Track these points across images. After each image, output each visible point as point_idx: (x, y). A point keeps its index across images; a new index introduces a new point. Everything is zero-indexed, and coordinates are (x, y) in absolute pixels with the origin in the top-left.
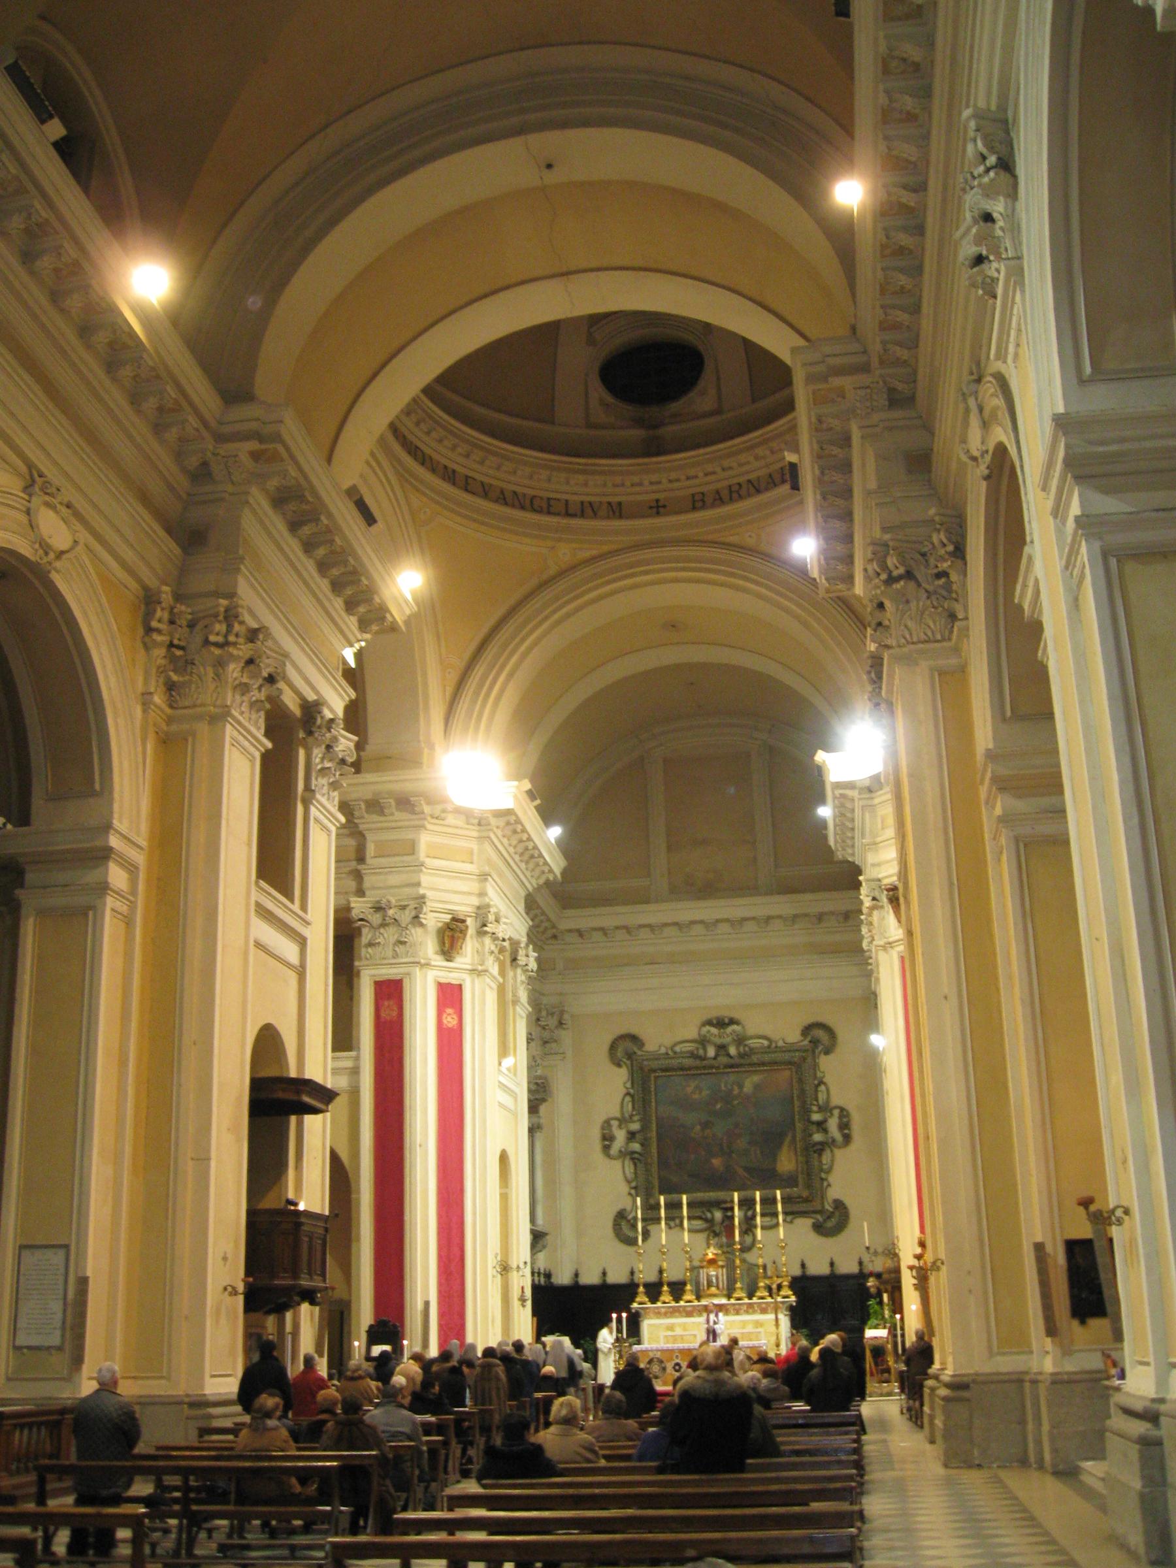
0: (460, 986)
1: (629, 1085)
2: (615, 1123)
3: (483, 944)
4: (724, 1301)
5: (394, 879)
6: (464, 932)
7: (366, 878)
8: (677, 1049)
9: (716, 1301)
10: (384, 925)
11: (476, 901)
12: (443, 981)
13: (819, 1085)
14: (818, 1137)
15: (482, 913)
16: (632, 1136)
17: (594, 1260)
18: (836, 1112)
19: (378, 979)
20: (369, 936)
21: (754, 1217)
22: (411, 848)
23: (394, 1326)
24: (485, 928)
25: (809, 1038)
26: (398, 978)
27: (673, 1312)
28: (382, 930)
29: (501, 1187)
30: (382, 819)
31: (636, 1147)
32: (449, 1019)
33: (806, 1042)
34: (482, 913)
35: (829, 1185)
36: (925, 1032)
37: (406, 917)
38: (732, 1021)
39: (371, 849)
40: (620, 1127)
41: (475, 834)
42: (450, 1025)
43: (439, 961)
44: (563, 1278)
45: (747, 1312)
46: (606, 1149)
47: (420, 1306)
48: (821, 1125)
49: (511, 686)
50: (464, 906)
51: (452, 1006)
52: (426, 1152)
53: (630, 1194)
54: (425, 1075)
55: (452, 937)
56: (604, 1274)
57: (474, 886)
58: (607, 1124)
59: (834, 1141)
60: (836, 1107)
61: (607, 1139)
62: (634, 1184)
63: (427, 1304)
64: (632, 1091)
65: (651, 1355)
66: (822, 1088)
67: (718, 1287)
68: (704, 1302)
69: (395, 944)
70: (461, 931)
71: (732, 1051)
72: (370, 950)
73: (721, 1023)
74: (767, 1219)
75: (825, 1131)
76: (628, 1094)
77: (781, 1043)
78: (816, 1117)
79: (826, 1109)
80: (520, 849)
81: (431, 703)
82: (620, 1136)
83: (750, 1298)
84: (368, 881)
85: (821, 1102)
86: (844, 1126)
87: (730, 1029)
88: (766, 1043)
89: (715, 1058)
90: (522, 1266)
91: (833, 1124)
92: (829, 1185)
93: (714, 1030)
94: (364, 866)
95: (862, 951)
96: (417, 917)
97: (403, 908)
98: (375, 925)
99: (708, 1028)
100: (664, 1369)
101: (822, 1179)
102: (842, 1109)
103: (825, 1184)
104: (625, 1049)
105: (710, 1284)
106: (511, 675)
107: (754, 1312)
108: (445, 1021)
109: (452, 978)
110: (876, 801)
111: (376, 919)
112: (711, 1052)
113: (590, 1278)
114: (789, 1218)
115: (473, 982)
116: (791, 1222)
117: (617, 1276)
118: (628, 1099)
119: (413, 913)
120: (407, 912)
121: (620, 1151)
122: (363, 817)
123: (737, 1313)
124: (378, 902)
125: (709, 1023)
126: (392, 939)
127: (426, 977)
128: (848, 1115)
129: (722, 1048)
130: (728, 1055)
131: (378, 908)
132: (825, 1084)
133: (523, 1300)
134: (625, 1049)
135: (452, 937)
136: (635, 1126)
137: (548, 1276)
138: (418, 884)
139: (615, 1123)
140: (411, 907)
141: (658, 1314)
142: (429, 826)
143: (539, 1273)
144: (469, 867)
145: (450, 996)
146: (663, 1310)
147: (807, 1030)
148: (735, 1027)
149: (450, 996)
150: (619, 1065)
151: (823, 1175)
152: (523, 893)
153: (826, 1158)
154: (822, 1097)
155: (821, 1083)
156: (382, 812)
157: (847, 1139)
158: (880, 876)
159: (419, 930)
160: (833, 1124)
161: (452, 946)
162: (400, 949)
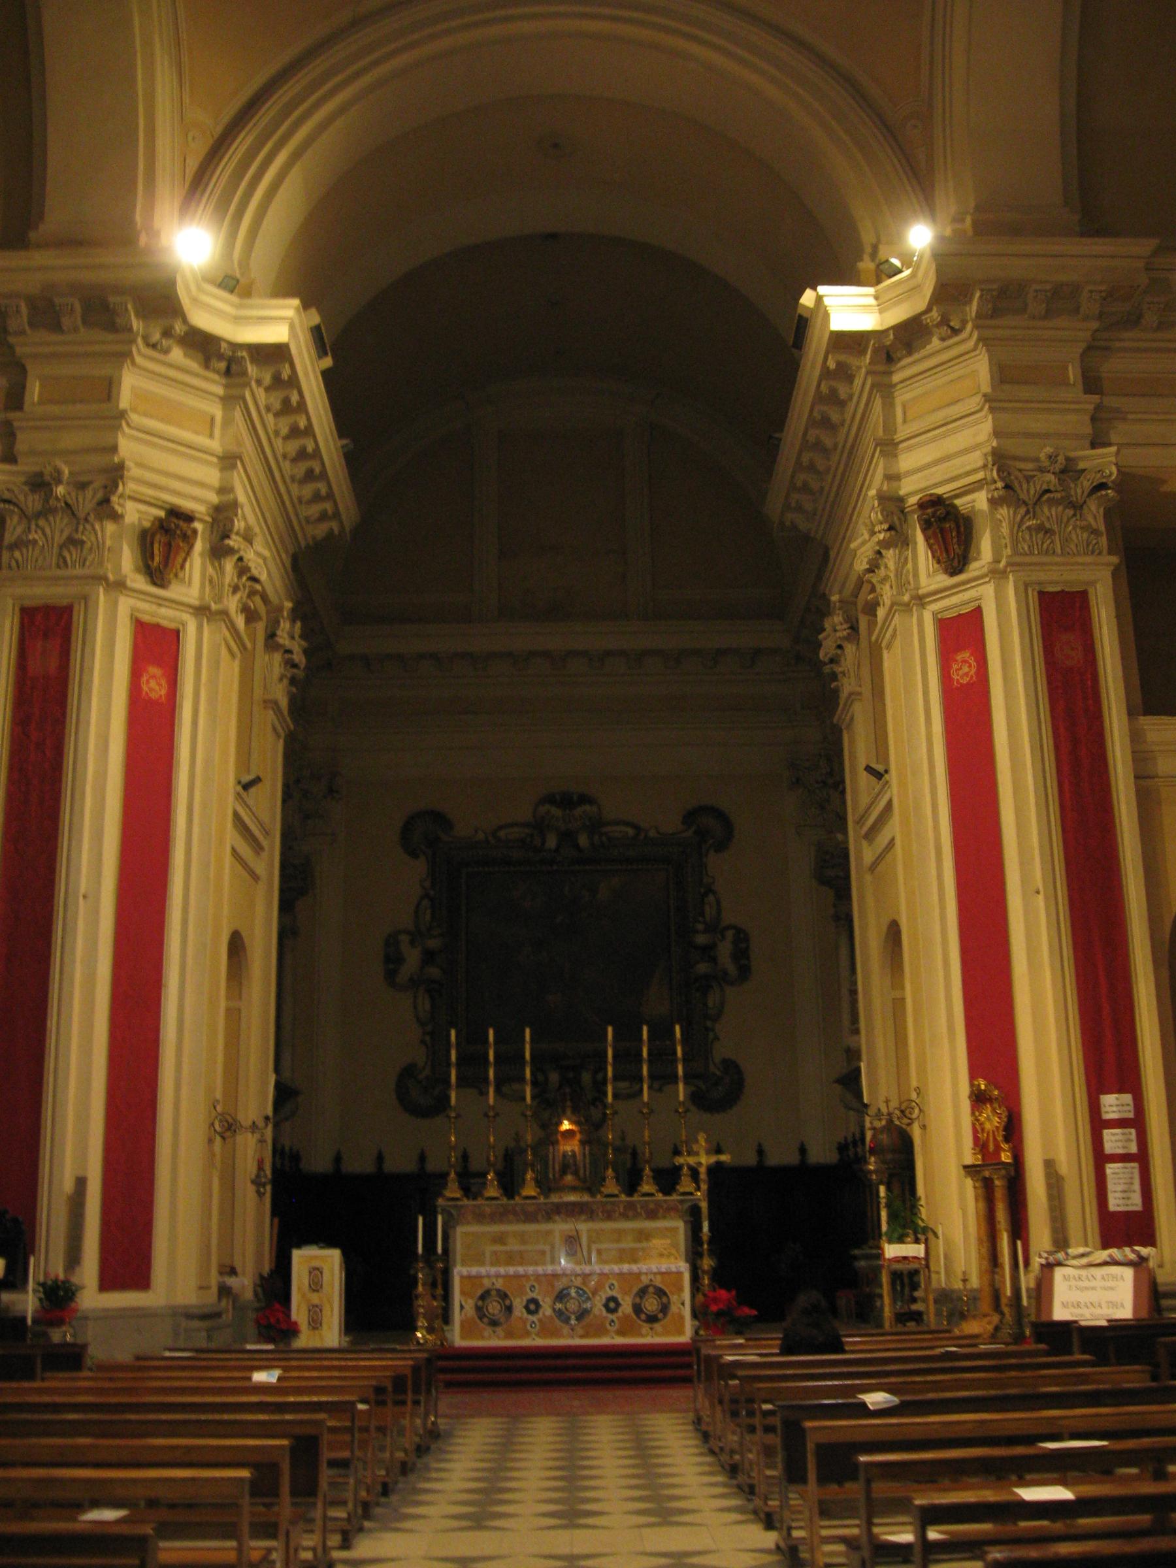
0: (177, 632)
1: (427, 884)
2: (404, 939)
3: (222, 569)
4: (586, 1198)
5: (71, 440)
6: (189, 538)
7: (20, 436)
8: (502, 834)
9: (572, 1198)
10: (46, 512)
11: (214, 498)
12: (146, 618)
13: (706, 894)
14: (702, 968)
15: (223, 514)
16: (429, 957)
17: (368, 1136)
18: (730, 934)
19: (28, 603)
20: (19, 530)
21: (604, 1082)
22: (108, 389)
23: (15, 1221)
24: (227, 542)
25: (693, 829)
26: (65, 602)
27: (500, 1216)
28: (42, 522)
29: (229, 997)
30: (54, 337)
31: (434, 972)
32: (153, 684)
33: (690, 833)
34: (223, 514)
35: (717, 1038)
36: (28, 1416)
37: (86, 502)
38: (584, 799)
39: (34, 391)
40: (412, 943)
41: (220, 391)
42: (153, 696)
43: (139, 582)
44: (318, 1162)
45: (624, 1216)
46: (390, 976)
47: (68, 1186)
48: (708, 951)
49: (295, 174)
50: (198, 501)
51: (159, 663)
52: (96, 911)
53: (423, 1042)
54: (102, 775)
55: (169, 545)
56: (422, 1158)
57: (212, 476)
58: (391, 941)
59: (726, 973)
60: (728, 928)
61: (392, 960)
62: (429, 1028)
63: (81, 1182)
64: (432, 893)
65: (487, 1283)
66: (711, 898)
67: (576, 1173)
68: (555, 1198)
69: (61, 547)
70: (185, 537)
71: (583, 840)
72: (17, 554)
73: (567, 801)
74: (623, 1085)
75: (714, 960)
76: (427, 896)
77: (652, 833)
78: (701, 939)
79: (715, 928)
80: (293, 447)
81: (159, 165)
82: (412, 957)
83: (630, 1194)
84: (21, 446)
85: (708, 918)
86: (741, 954)
87: (578, 811)
88: (631, 831)
89: (557, 850)
90: (261, 1124)
91: (725, 950)
92: (717, 1038)
93: (556, 812)
94: (18, 414)
95: (817, 665)
96: (106, 501)
97: (82, 486)
98: (29, 512)
99: (547, 807)
100: (509, 1309)
101: (707, 1029)
102: (739, 931)
103: (711, 1035)
104: (425, 832)
105: (564, 1169)
106: (296, 156)
107: (636, 1216)
108: (145, 688)
109: (165, 616)
110: (896, 378)
111: (33, 502)
112: (552, 842)
113: (359, 1164)
114: (656, 1085)
115: (200, 629)
116: (660, 1090)
117: (400, 1162)
118: (425, 902)
119: (100, 495)
120: (89, 493)
121: (411, 979)
122: (23, 332)
123: (609, 1216)
124: (41, 474)
125: (550, 799)
126: (58, 539)
127: (115, 604)
128: (747, 939)
129: (567, 837)
130: (577, 847)
131: (40, 484)
132: (714, 893)
133: (257, 1182)
134: (425, 832)
135: (169, 545)
136: (434, 944)
137: (295, 1158)
138: (114, 449)
139: (404, 939)
140: (97, 484)
141: (480, 1218)
142: (139, 360)
143: (282, 1153)
144: (202, 440)
145: (156, 646)
146: (488, 1210)
147: (690, 817)
148: (587, 807)
149: (156, 646)
150: (414, 854)
151: (709, 1024)
152: (291, 550)
153: (712, 999)
154: (709, 912)
155: (710, 891)
156: (57, 327)
157: (745, 972)
158: (902, 493)
159: (110, 527)
160: (725, 950)
161: (167, 560)
162: (71, 555)
